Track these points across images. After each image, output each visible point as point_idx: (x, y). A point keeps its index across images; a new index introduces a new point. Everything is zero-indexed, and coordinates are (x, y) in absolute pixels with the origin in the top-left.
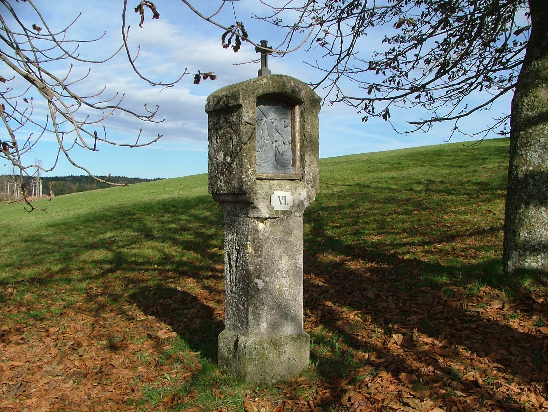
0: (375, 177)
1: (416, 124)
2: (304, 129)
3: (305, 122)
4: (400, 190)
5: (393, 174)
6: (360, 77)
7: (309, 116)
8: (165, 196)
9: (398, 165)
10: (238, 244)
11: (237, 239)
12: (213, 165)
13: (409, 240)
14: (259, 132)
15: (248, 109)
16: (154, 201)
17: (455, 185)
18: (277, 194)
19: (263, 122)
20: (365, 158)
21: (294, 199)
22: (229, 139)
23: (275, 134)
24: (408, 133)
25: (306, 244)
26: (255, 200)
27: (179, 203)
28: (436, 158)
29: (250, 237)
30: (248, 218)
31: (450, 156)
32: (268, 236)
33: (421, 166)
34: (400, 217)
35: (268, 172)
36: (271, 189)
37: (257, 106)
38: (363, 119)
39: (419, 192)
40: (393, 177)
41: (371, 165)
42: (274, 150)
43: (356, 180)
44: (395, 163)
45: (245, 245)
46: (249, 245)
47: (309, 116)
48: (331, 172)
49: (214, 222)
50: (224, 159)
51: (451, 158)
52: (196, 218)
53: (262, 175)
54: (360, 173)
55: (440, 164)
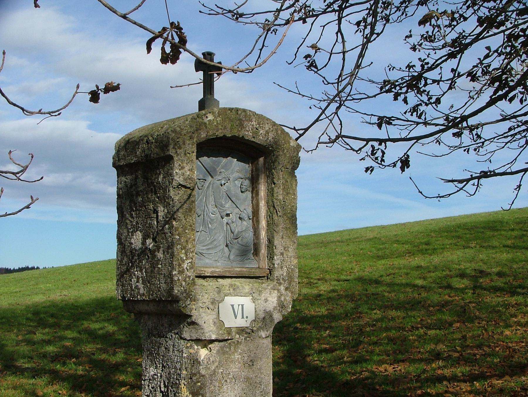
0: (388, 266)
1: (455, 183)
2: (273, 196)
3: (274, 184)
4: (430, 287)
5: (418, 260)
6: (364, 106)
7: (281, 173)
8: (39, 299)
9: (427, 247)
10: (164, 384)
11: (164, 375)
12: (124, 254)
13: (447, 372)
14: (201, 200)
15: (182, 163)
16: (18, 306)
17: (523, 279)
18: (230, 300)
19: (207, 184)
20: (371, 235)
21: (257, 309)
22: (152, 212)
23: (226, 203)
24: (443, 197)
25: (277, 380)
26: (194, 311)
27: (62, 309)
28: (489, 233)
29: (184, 372)
30: (182, 341)
31: (513, 230)
32: (214, 370)
33: (464, 247)
34: (432, 332)
35: (215, 265)
36: (219, 292)
37: (197, 159)
38: (367, 169)
39: (462, 291)
40: (418, 267)
41: (381, 247)
42: (225, 230)
43: (357, 271)
44: (421, 243)
45: (177, 386)
46: (183, 386)
47: (281, 173)
48: (314, 257)
49: (122, 343)
50: (144, 243)
51: (515, 233)
52: (93, 336)
53: (205, 269)
54: (364, 260)
55: (495, 243)
